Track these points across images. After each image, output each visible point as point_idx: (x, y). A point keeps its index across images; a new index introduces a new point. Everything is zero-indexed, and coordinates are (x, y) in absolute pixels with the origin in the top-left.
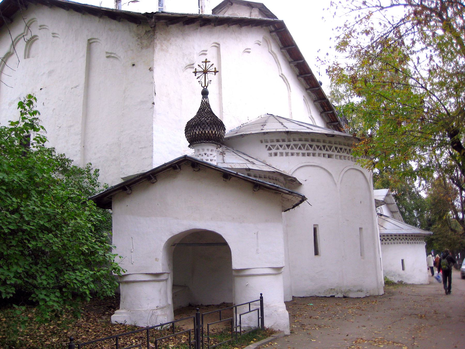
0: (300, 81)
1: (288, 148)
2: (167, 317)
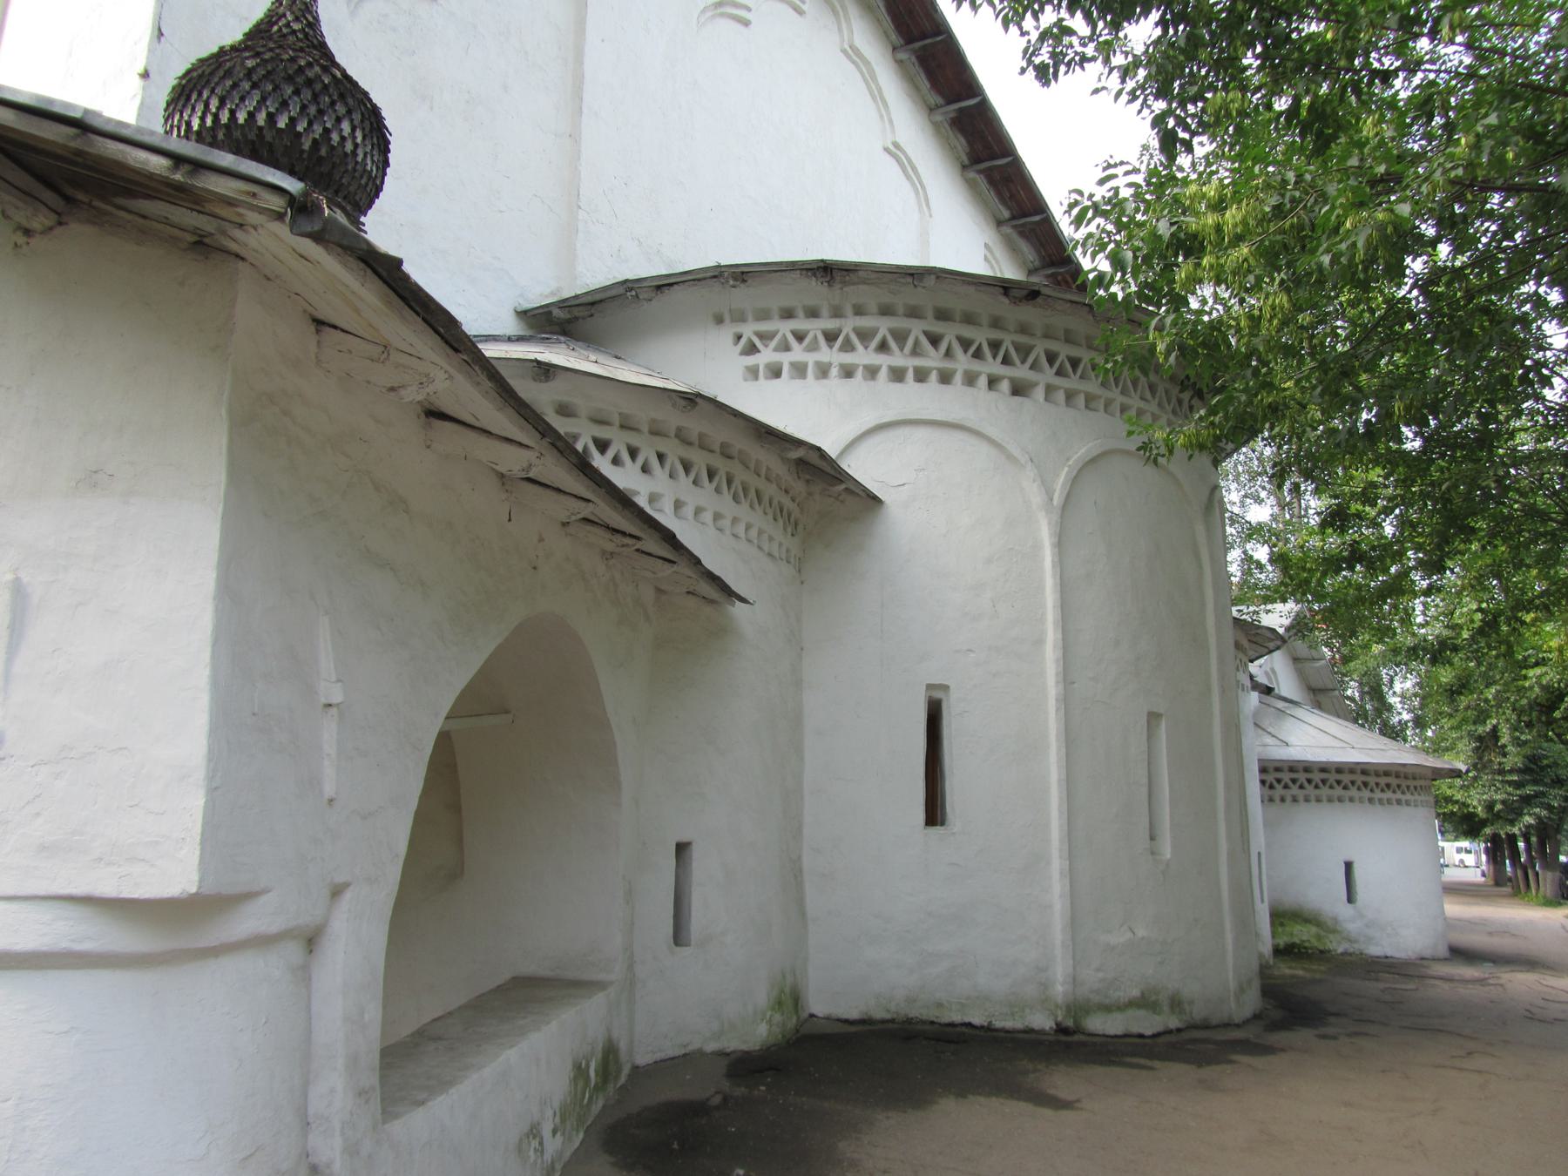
0: (971, 185)
1: (831, 347)
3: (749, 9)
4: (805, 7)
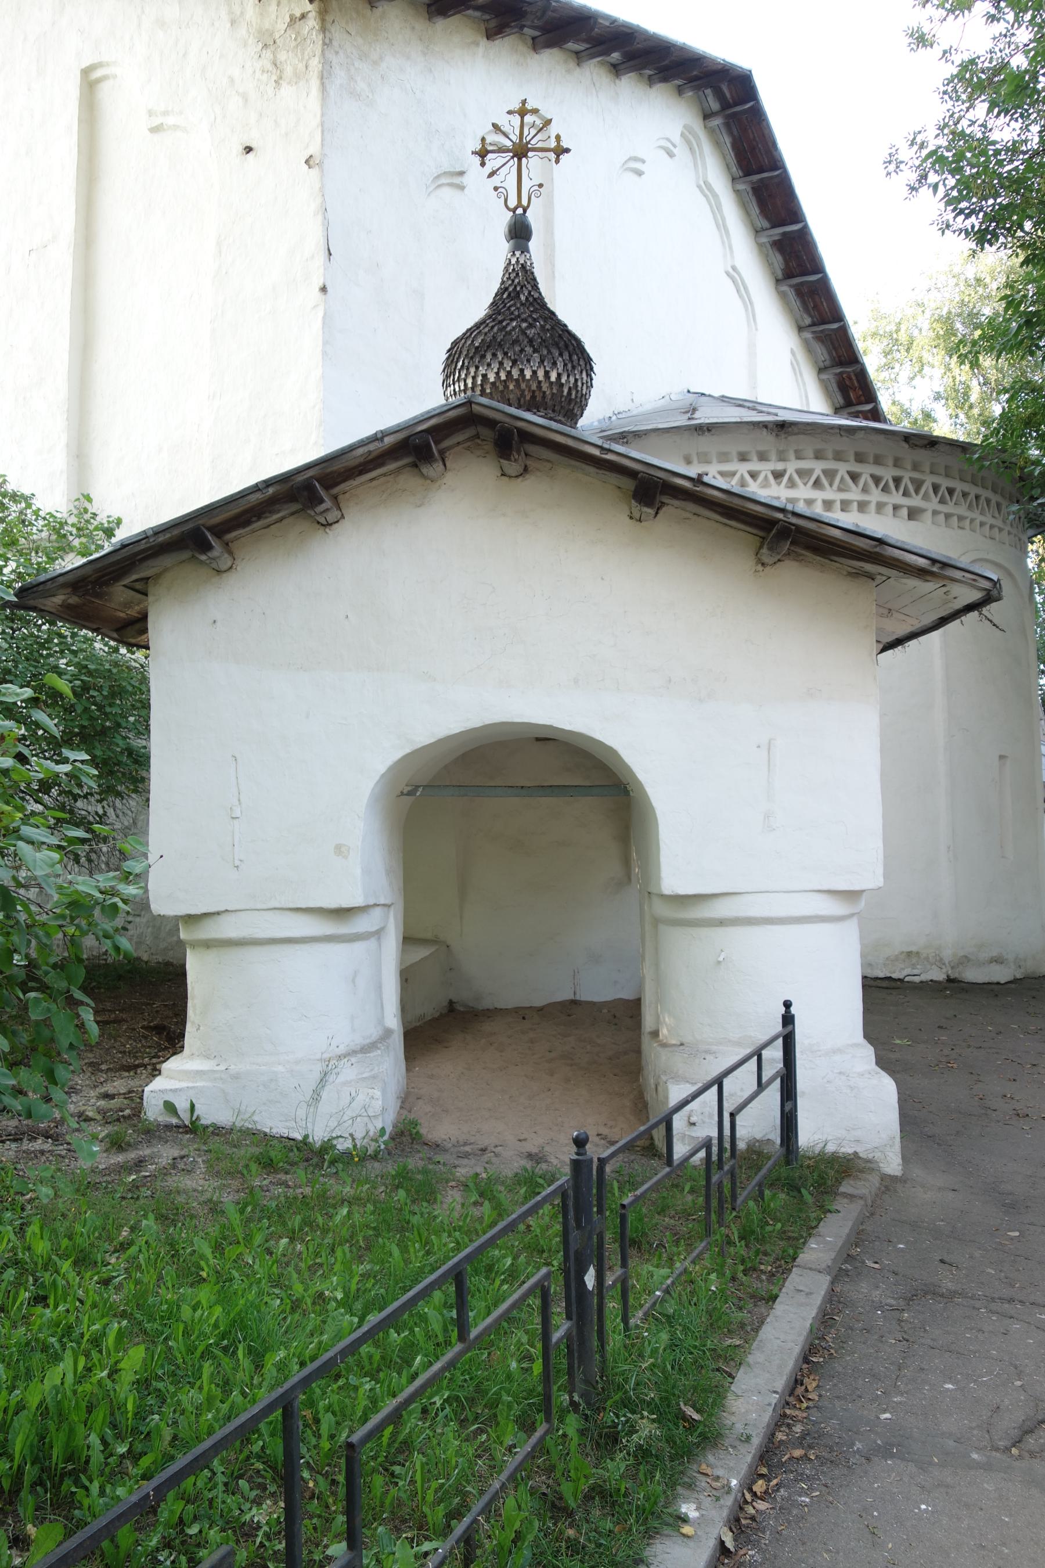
0: (782, 296)
1: (779, 484)
2: (384, 1092)
3: (643, 162)
4: (675, 151)
